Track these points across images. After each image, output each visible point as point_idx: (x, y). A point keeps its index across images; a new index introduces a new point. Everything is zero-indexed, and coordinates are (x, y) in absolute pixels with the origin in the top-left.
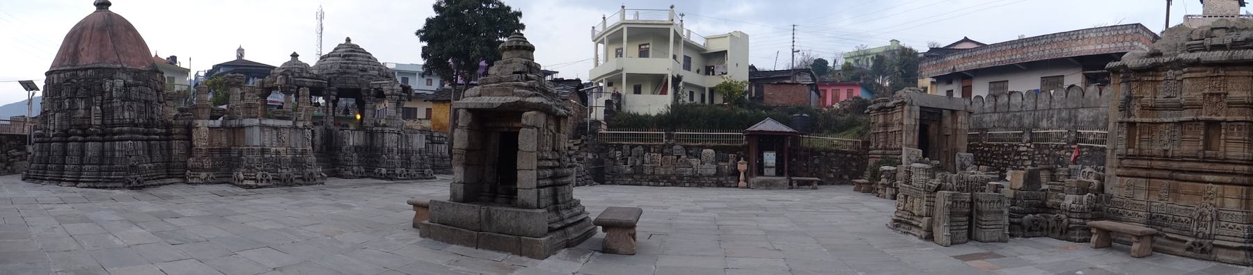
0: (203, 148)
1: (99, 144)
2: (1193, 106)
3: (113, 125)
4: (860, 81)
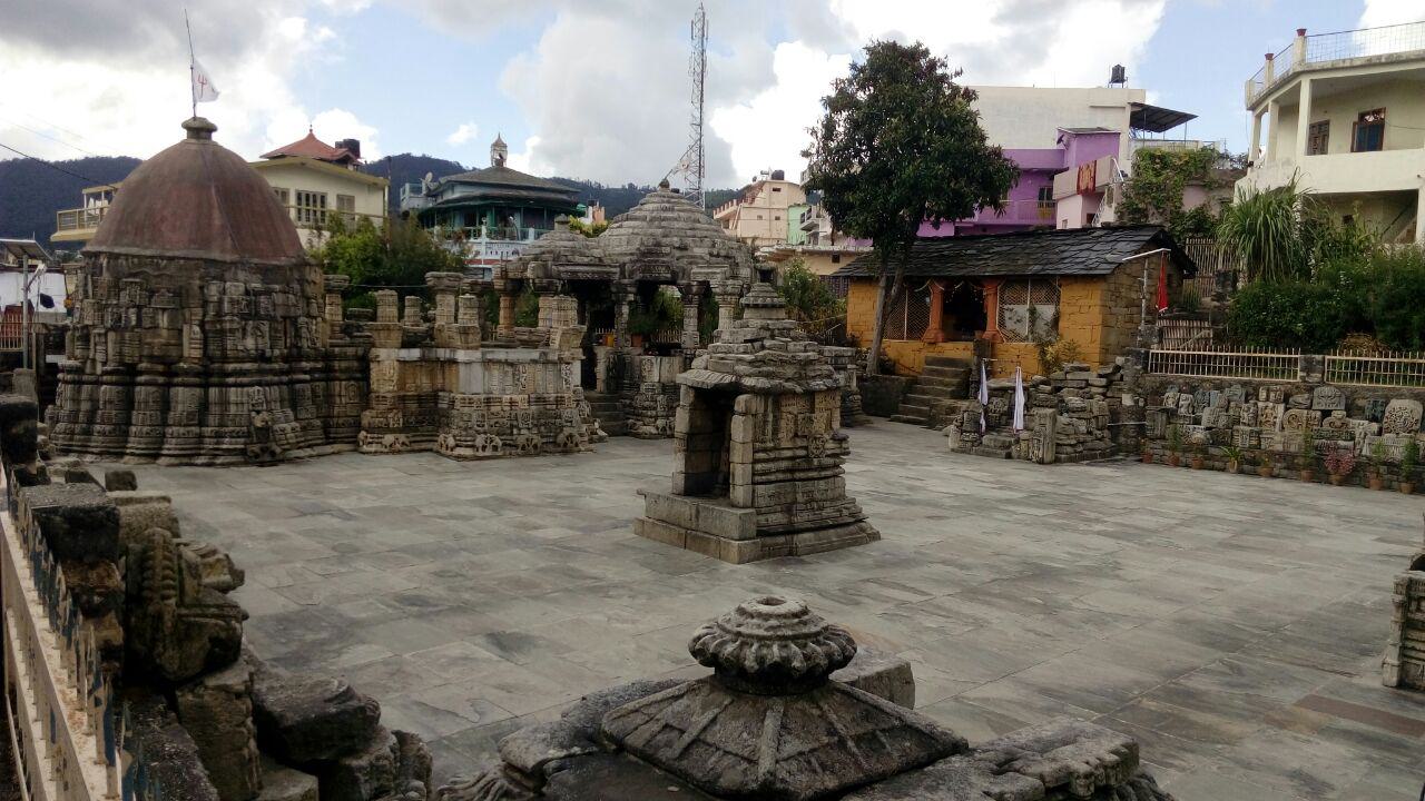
0: (389, 395)
1: (198, 391)
3: (225, 359)
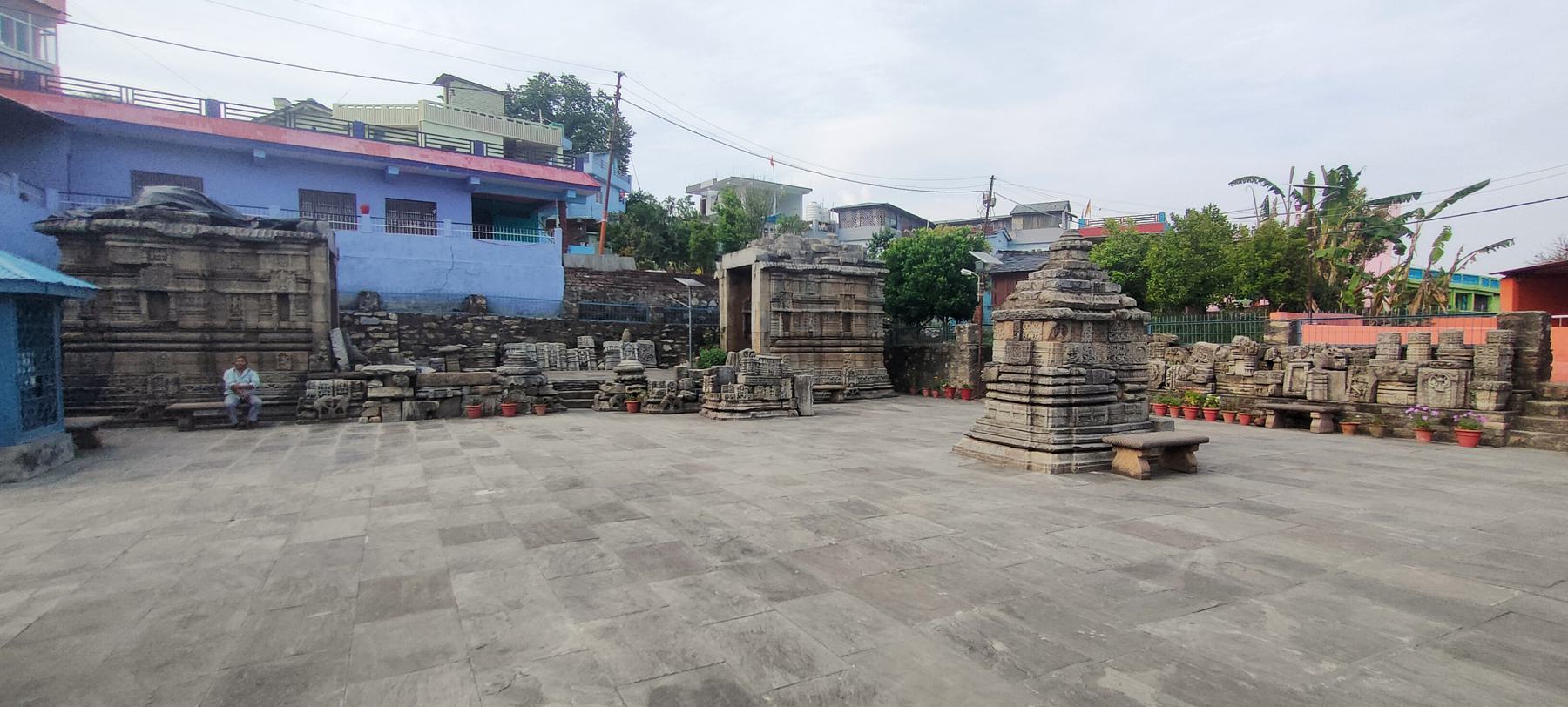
2: (835, 302)
4: (222, 399)
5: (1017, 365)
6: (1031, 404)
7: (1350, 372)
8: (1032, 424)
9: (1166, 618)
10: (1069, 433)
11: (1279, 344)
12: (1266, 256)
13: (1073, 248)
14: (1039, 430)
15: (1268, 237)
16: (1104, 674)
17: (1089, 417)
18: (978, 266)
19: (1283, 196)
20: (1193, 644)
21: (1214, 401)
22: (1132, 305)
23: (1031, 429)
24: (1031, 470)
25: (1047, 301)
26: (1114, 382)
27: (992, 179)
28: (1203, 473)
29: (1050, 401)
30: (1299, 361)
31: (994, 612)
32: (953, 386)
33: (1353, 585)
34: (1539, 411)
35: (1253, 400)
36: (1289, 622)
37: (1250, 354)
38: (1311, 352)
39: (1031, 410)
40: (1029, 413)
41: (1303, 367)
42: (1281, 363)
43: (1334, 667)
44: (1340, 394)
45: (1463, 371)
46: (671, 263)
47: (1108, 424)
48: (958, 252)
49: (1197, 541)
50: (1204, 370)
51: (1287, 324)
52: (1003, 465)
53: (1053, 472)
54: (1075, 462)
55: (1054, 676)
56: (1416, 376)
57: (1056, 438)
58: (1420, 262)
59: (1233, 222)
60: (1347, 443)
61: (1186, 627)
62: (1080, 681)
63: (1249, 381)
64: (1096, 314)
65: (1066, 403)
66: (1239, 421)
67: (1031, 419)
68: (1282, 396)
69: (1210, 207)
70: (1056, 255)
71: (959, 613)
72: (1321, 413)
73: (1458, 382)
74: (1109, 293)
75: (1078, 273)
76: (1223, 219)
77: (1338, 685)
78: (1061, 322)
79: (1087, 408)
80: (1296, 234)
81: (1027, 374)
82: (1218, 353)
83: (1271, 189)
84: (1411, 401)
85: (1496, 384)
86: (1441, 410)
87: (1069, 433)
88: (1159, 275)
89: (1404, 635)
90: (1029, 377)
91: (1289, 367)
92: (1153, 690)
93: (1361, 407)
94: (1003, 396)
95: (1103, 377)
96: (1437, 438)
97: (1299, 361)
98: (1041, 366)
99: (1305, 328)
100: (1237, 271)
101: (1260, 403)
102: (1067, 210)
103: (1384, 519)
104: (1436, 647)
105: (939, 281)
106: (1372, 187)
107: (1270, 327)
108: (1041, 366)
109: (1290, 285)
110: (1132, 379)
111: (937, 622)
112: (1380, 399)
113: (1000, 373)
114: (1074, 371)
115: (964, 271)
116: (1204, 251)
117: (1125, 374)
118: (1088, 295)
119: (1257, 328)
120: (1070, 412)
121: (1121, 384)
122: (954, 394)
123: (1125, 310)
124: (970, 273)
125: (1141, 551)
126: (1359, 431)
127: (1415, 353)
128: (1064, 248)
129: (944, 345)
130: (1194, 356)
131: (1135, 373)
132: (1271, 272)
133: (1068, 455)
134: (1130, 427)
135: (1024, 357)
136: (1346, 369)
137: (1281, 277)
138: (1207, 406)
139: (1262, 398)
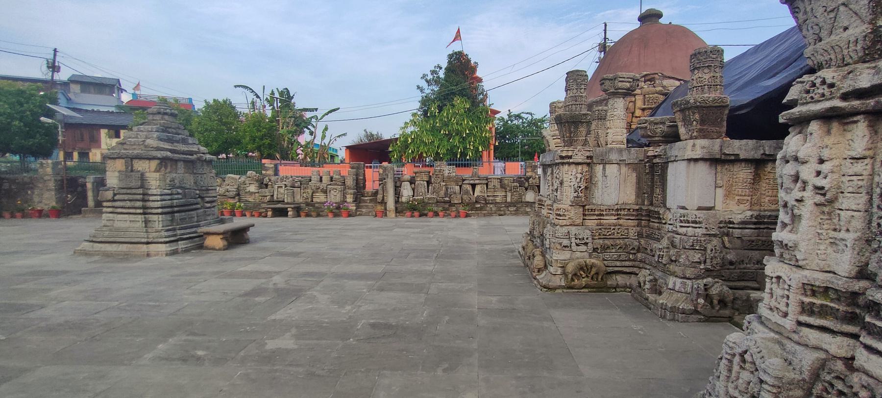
5: (130, 188)
6: (144, 214)
7: (302, 188)
8: (146, 227)
9: (279, 310)
10: (174, 230)
11: (270, 175)
12: (258, 130)
13: (165, 114)
14: (152, 230)
15: (258, 121)
16: (266, 343)
17: (185, 219)
18: (59, 117)
19: (261, 100)
20: (297, 317)
21: (240, 206)
22: (206, 152)
23: (146, 230)
24: (151, 256)
25: (151, 146)
26: (198, 197)
27: (55, 50)
28: (252, 242)
29: (160, 211)
30: (279, 183)
31: (184, 337)
32: (39, 208)
33: (343, 276)
34: (365, 201)
35: (260, 204)
36: (327, 296)
37: (257, 181)
38: (285, 180)
39: (145, 218)
40: (143, 220)
41: (282, 187)
42: (271, 185)
43: (350, 307)
44: (299, 199)
45: (342, 186)
46: (438, 125)
47: (197, 222)
48: (33, 103)
49: (269, 274)
50: (233, 189)
51: (273, 165)
52: (126, 257)
53: (167, 255)
54: (180, 247)
55: (242, 354)
56: (327, 190)
57: (166, 234)
58: (318, 141)
59: (239, 110)
60: (303, 221)
61: (289, 311)
62: (257, 351)
63: (257, 195)
64: (185, 156)
65: (170, 211)
66: (254, 215)
67: (145, 223)
68: (273, 202)
69: (227, 100)
70: (154, 116)
71: (160, 346)
72: (292, 208)
73: (341, 191)
74: (191, 144)
75: (170, 130)
76: (234, 108)
77: (354, 313)
78: (164, 161)
79: (183, 214)
80: (271, 121)
81: (140, 194)
82: (240, 180)
83: (255, 95)
84: (326, 200)
85: (352, 191)
86: (336, 203)
87: (174, 230)
88: (201, 135)
89: (364, 289)
90: (141, 196)
91: (276, 187)
92: (292, 341)
93: (308, 204)
94: (119, 210)
95: (192, 194)
96: (336, 215)
97: (279, 183)
98: (150, 189)
99: (280, 168)
100: (244, 137)
101: (264, 205)
102: (118, 85)
103: (336, 249)
104: (373, 290)
105: (15, 125)
106: (299, 103)
107: (265, 167)
108: (150, 189)
109: (270, 146)
110: (208, 195)
111: (150, 355)
112: (314, 200)
113: (115, 195)
114: (174, 191)
115: (43, 119)
116: (225, 124)
117: (204, 192)
118: (178, 144)
119: (260, 168)
120: (173, 217)
121: (202, 198)
122: (40, 214)
123: (202, 155)
124: (50, 121)
125: (248, 285)
126: (308, 215)
127: (326, 179)
128: (159, 113)
129: (25, 177)
130: (227, 182)
131: (210, 192)
132: (262, 139)
133: (175, 243)
134: (210, 222)
135: (136, 183)
136: (300, 187)
137: (267, 141)
138: (237, 209)
139: (264, 203)
